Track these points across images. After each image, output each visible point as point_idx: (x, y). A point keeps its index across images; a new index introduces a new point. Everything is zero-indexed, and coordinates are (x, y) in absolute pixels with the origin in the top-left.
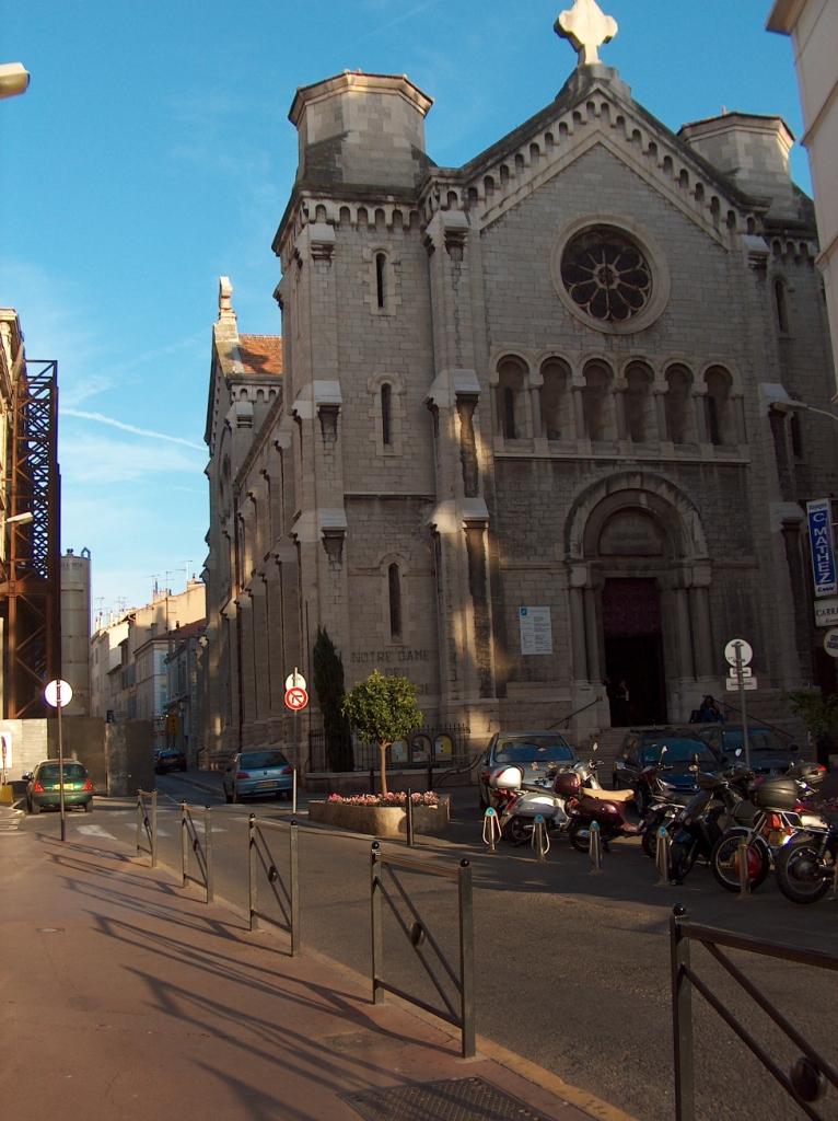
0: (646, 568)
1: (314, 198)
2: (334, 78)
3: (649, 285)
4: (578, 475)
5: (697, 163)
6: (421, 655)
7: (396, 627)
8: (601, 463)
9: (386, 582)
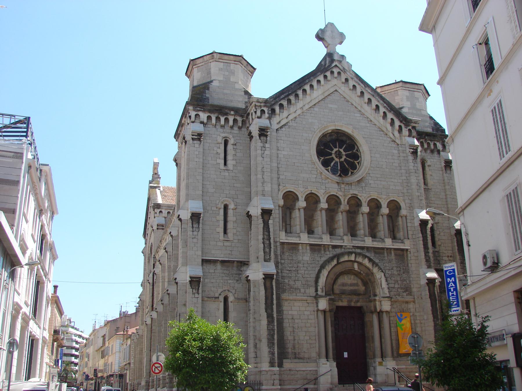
1: (194, 110)
9: (222, 305)
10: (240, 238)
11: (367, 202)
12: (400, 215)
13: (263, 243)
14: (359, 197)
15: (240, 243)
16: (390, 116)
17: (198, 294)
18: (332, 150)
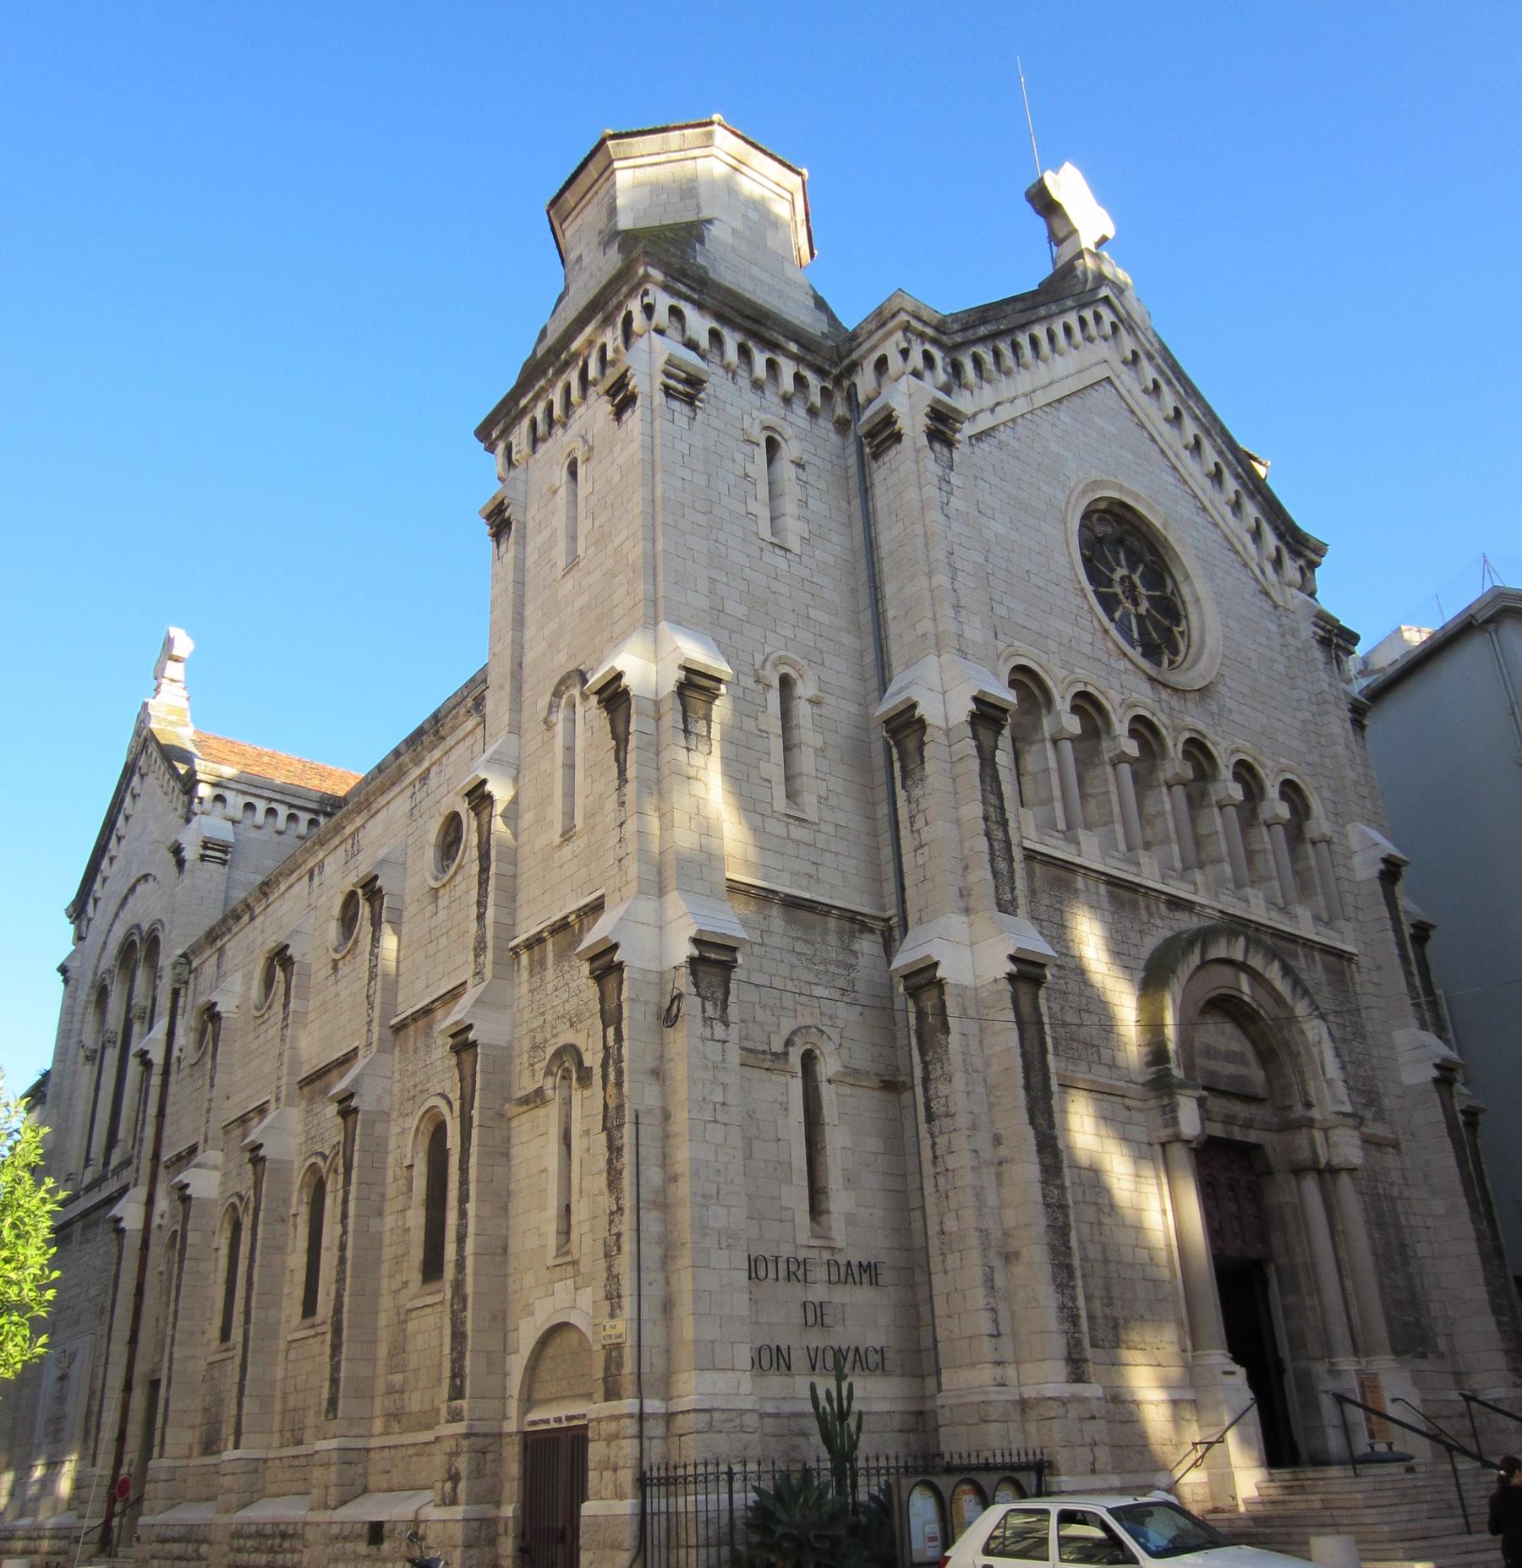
0: (1248, 1124)
1: (666, 288)
2: (687, 127)
3: (1184, 623)
4: (1145, 918)
5: (1236, 457)
6: (868, 1272)
7: (816, 1210)
8: (1175, 903)
9: (797, 1086)
10: (841, 818)
11: (1231, 767)
12: (1308, 836)
13: (988, 834)
14: (1210, 746)
15: (842, 839)
16: (1251, 510)
17: (726, 1024)
18: (1112, 570)
